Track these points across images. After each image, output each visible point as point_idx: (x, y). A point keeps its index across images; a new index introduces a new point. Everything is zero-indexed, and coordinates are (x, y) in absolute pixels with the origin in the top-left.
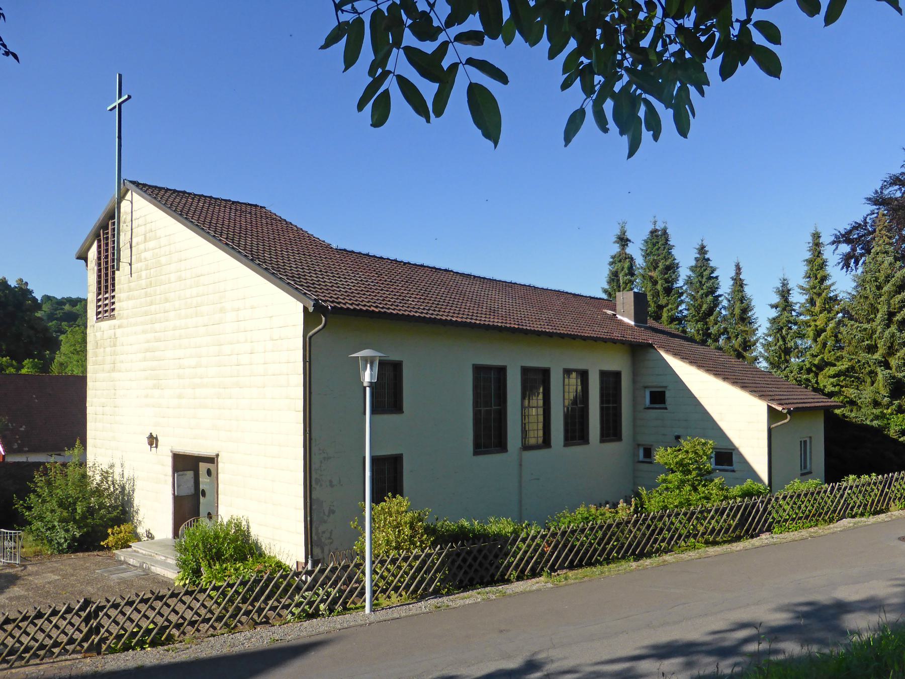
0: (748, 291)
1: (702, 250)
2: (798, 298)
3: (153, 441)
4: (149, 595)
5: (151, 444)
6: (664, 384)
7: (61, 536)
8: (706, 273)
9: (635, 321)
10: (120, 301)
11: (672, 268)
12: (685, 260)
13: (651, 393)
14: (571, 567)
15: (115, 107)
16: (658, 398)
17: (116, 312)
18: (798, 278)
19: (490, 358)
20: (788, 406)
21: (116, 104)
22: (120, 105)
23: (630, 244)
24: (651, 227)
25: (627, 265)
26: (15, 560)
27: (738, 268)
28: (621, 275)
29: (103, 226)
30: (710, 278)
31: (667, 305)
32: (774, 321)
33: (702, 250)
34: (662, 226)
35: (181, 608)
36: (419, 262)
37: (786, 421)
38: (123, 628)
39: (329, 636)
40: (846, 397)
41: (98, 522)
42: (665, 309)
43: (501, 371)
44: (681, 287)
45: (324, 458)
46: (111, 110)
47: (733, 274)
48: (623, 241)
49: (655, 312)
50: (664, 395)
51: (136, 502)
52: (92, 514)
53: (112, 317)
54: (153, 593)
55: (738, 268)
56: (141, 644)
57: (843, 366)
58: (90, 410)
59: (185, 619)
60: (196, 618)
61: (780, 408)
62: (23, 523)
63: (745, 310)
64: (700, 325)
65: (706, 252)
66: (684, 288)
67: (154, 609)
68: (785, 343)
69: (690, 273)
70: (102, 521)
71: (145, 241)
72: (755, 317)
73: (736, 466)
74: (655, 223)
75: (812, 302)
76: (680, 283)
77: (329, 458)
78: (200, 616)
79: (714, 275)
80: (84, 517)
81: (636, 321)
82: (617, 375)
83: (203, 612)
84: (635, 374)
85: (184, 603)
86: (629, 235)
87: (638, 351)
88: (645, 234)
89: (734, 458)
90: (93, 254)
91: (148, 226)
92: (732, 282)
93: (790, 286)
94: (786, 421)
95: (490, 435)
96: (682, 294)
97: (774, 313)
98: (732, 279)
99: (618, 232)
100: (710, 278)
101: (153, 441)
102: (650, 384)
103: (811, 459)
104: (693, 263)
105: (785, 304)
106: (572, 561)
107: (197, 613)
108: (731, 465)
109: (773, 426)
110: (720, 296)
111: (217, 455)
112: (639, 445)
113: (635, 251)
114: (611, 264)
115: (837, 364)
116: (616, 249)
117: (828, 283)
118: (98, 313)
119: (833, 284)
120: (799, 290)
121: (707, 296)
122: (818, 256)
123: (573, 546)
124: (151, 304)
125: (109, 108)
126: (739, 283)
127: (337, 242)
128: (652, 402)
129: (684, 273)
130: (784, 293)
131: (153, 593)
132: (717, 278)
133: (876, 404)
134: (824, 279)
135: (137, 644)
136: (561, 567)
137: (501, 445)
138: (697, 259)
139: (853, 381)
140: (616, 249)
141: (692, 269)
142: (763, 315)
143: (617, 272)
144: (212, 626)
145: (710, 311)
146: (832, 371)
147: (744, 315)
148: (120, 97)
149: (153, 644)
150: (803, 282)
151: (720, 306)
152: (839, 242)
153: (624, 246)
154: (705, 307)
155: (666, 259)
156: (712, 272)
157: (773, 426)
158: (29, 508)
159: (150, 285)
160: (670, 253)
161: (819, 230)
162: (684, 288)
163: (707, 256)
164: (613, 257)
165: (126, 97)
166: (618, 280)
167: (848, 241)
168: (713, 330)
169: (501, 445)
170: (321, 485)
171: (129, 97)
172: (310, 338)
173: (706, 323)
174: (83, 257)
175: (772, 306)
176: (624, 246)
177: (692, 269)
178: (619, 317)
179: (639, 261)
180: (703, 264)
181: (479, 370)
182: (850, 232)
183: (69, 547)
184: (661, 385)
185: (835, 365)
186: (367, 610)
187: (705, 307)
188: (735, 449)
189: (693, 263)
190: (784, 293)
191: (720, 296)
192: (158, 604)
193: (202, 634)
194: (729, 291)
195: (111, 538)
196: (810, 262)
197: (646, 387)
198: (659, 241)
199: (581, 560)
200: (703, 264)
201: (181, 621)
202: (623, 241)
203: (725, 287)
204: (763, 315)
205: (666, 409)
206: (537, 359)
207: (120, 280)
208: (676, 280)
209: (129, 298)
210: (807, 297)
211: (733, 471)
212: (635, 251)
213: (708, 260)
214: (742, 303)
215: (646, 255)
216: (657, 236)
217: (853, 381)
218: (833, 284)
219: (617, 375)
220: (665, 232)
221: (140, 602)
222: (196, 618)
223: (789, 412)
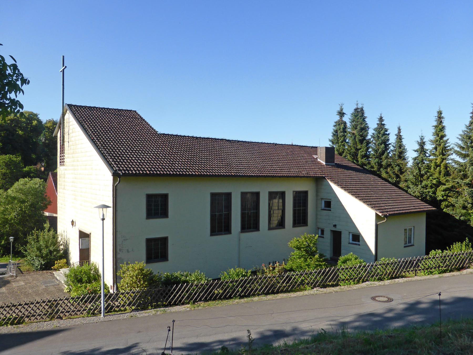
0: (404, 142)
1: (381, 119)
2: (429, 147)
3: (73, 223)
4: (9, 305)
5: (73, 225)
6: (330, 198)
7: (37, 263)
8: (382, 132)
9: (326, 162)
11: (365, 129)
12: (372, 124)
13: (325, 202)
14: (206, 300)
16: (328, 204)
18: (429, 136)
19: (221, 188)
20: (386, 213)
21: (62, 70)
22: (63, 70)
23: (345, 115)
24: (355, 107)
25: (342, 126)
27: (399, 129)
28: (339, 132)
30: (384, 134)
31: (360, 149)
32: (415, 159)
33: (381, 119)
35: (23, 310)
36: (206, 136)
37: (384, 221)
38: (17, 315)
39: (65, 328)
40: (449, 202)
41: (52, 257)
42: (360, 151)
43: (228, 196)
44: (370, 139)
45: (124, 240)
47: (397, 132)
48: (341, 114)
49: (354, 152)
50: (330, 203)
51: (70, 249)
52: (51, 254)
54: (11, 304)
55: (399, 129)
56: (6, 324)
57: (449, 185)
58: (59, 205)
59: (25, 315)
60: (29, 314)
61: (380, 214)
62: (23, 256)
63: (401, 153)
64: (377, 160)
65: (383, 121)
66: (372, 139)
67: (12, 310)
68: (420, 171)
69: (374, 132)
70: (53, 257)
72: (407, 156)
73: (360, 243)
74: (357, 104)
75: (436, 148)
76: (369, 137)
77: (126, 240)
78: (31, 314)
79: (387, 133)
80: (47, 255)
81: (326, 162)
82: (306, 193)
83: (32, 312)
84: (317, 191)
85: (25, 308)
86: (344, 111)
87: (319, 181)
88: (352, 111)
89: (360, 239)
92: (396, 137)
93: (424, 141)
94: (384, 221)
95: (220, 225)
96: (370, 143)
97: (415, 155)
98: (396, 135)
99: (339, 109)
100: (384, 134)
102: (325, 197)
103: (414, 238)
104: (376, 126)
105: (422, 149)
106: (206, 298)
107: (30, 312)
108: (359, 242)
109: (378, 223)
110: (390, 144)
111: (90, 234)
112: (319, 228)
113: (347, 119)
114: (335, 126)
115: (447, 184)
116: (337, 118)
117: (445, 139)
118: (60, 162)
119: (448, 139)
120: (430, 143)
121: (381, 144)
122: (440, 124)
126: (399, 138)
127: (161, 129)
129: (371, 132)
130: (422, 144)
131: (11, 304)
132: (389, 134)
133: (464, 207)
134: (442, 137)
135: (5, 324)
136: (200, 300)
137: (227, 229)
139: (455, 194)
140: (337, 118)
141: (375, 130)
142: (411, 154)
143: (337, 131)
144: (36, 318)
145: (383, 153)
146: (444, 187)
147: (401, 154)
148: (63, 66)
149: (12, 324)
150: (432, 138)
151: (389, 150)
153: (341, 116)
154: (380, 150)
155: (361, 124)
156: (386, 131)
157: (378, 223)
158: (26, 251)
159: (73, 153)
160: (365, 121)
161: (441, 109)
162: (372, 139)
163: (383, 123)
164: (335, 123)
166: (337, 135)
168: (384, 163)
169: (227, 229)
170: (122, 252)
172: (116, 186)
173: (381, 159)
175: (415, 151)
176: (341, 116)
177: (375, 130)
178: (319, 160)
179: (348, 125)
180: (381, 127)
181: (214, 196)
183: (41, 268)
184: (328, 198)
185: (445, 185)
186: (102, 316)
187: (380, 150)
188: (360, 234)
189: (376, 126)
190: (422, 144)
191: (390, 144)
192: (13, 308)
193: (32, 321)
194: (394, 141)
195: (56, 265)
196: (436, 127)
197: (322, 199)
198: (359, 114)
199: (211, 297)
200: (381, 127)
201: (23, 315)
202: (341, 114)
203: (392, 139)
204: (411, 154)
205: (330, 210)
206: (251, 187)
208: (367, 135)
209: (68, 158)
210: (434, 146)
211: (359, 245)
212: (347, 119)
213: (384, 125)
214: (400, 148)
215: (353, 121)
216: (358, 112)
217: (455, 194)
218: (448, 139)
219: (306, 193)
220: (362, 109)
221: (6, 307)
222: (29, 314)
223: (386, 216)
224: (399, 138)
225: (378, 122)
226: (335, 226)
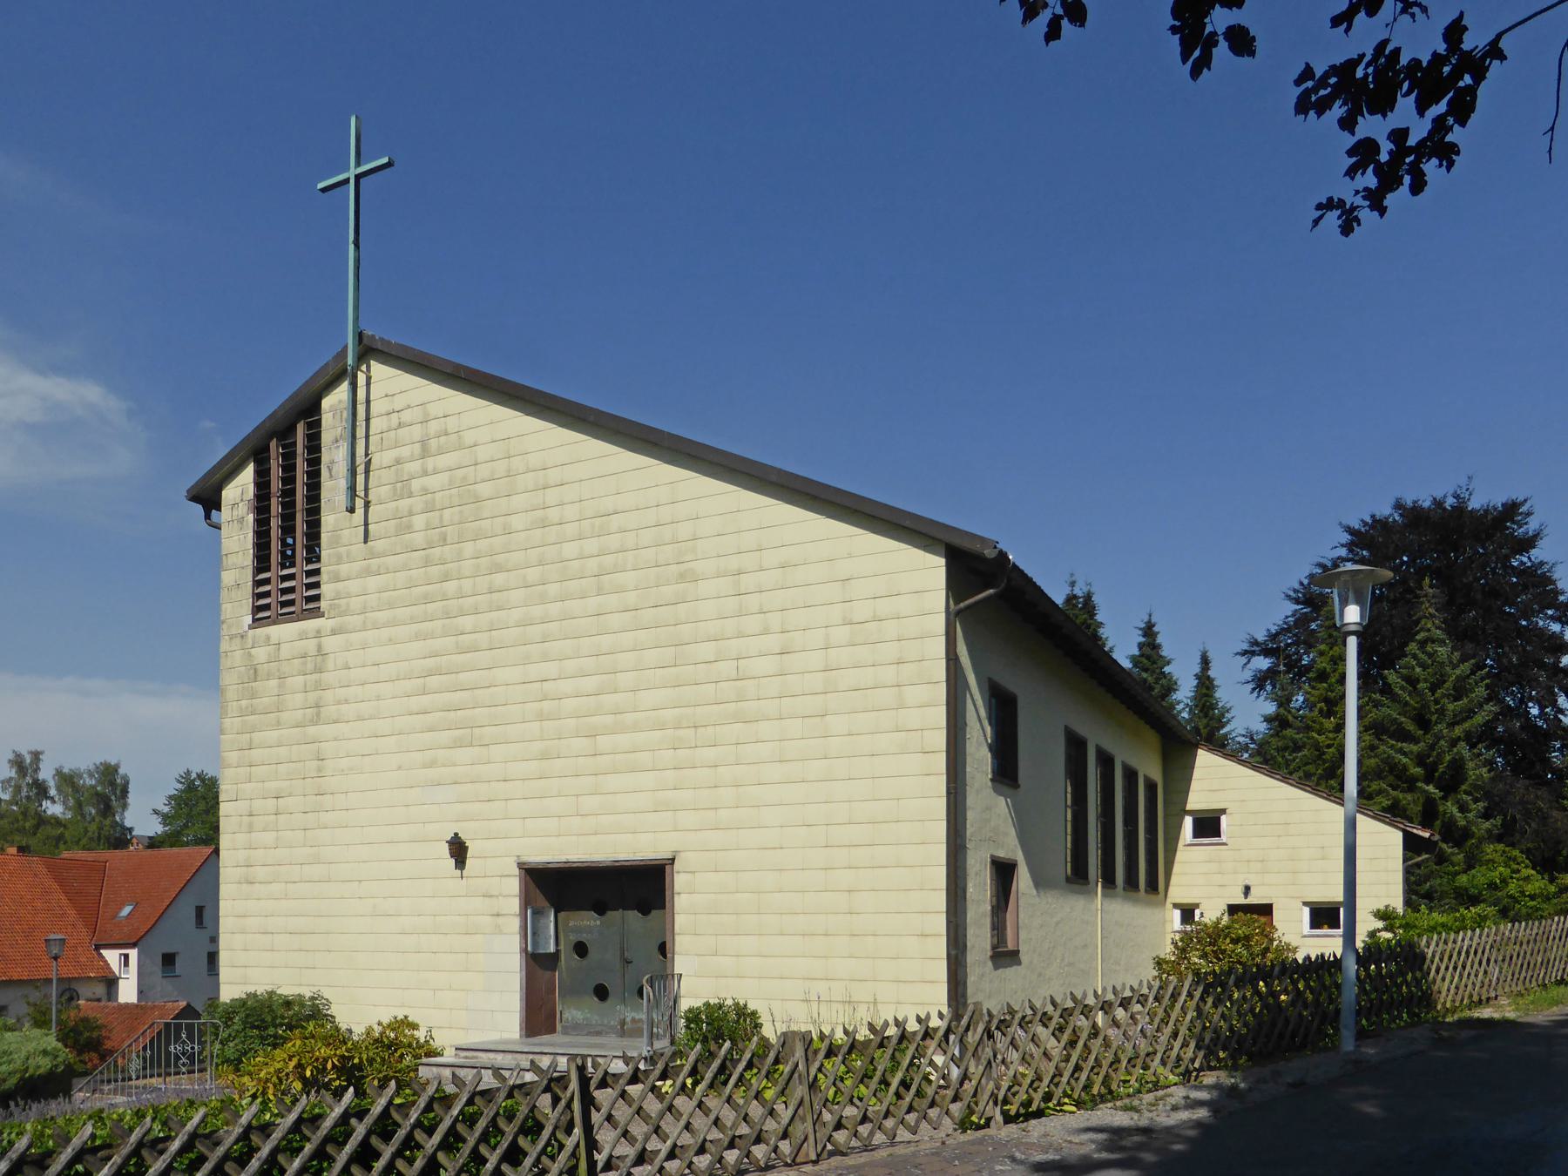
1: (1149, 631)
3: (458, 850)
10: (337, 579)
15: (347, 181)
17: (323, 604)
22: (358, 177)
26: (640, 1020)
27: (1205, 662)
29: (281, 429)
33: (1149, 631)
34: (1085, 590)
46: (324, 190)
47: (1197, 669)
53: (316, 613)
55: (1205, 662)
71: (425, 453)
74: (1073, 584)
90: (242, 487)
91: (434, 426)
101: (458, 850)
111: (673, 860)
123: (152, 1066)
124: (446, 578)
125: (321, 185)
126: (1205, 684)
128: (1196, 835)
138: (1141, 646)
148: (358, 164)
152: (1253, 653)
165: (385, 160)
167: (1266, 652)
171: (389, 164)
174: (208, 497)
182: (1273, 637)
203: (1184, 693)
207: (336, 542)
220: (1088, 597)
224: (1205, 684)
225: (1142, 639)
226: (1247, 889)
